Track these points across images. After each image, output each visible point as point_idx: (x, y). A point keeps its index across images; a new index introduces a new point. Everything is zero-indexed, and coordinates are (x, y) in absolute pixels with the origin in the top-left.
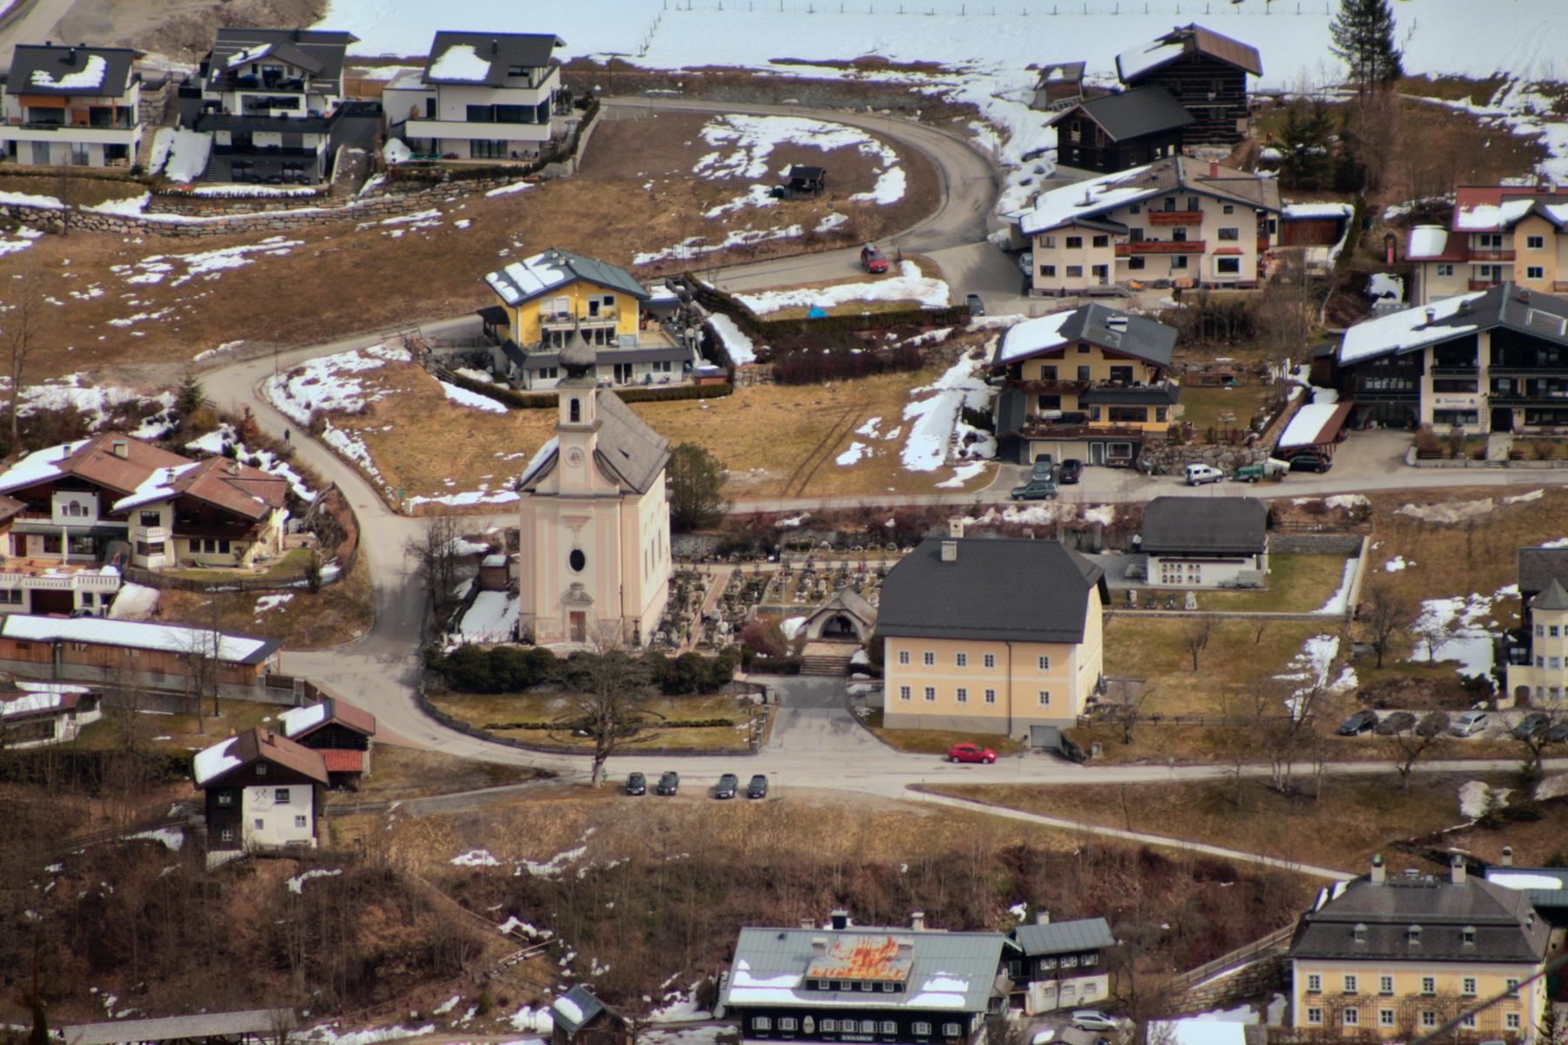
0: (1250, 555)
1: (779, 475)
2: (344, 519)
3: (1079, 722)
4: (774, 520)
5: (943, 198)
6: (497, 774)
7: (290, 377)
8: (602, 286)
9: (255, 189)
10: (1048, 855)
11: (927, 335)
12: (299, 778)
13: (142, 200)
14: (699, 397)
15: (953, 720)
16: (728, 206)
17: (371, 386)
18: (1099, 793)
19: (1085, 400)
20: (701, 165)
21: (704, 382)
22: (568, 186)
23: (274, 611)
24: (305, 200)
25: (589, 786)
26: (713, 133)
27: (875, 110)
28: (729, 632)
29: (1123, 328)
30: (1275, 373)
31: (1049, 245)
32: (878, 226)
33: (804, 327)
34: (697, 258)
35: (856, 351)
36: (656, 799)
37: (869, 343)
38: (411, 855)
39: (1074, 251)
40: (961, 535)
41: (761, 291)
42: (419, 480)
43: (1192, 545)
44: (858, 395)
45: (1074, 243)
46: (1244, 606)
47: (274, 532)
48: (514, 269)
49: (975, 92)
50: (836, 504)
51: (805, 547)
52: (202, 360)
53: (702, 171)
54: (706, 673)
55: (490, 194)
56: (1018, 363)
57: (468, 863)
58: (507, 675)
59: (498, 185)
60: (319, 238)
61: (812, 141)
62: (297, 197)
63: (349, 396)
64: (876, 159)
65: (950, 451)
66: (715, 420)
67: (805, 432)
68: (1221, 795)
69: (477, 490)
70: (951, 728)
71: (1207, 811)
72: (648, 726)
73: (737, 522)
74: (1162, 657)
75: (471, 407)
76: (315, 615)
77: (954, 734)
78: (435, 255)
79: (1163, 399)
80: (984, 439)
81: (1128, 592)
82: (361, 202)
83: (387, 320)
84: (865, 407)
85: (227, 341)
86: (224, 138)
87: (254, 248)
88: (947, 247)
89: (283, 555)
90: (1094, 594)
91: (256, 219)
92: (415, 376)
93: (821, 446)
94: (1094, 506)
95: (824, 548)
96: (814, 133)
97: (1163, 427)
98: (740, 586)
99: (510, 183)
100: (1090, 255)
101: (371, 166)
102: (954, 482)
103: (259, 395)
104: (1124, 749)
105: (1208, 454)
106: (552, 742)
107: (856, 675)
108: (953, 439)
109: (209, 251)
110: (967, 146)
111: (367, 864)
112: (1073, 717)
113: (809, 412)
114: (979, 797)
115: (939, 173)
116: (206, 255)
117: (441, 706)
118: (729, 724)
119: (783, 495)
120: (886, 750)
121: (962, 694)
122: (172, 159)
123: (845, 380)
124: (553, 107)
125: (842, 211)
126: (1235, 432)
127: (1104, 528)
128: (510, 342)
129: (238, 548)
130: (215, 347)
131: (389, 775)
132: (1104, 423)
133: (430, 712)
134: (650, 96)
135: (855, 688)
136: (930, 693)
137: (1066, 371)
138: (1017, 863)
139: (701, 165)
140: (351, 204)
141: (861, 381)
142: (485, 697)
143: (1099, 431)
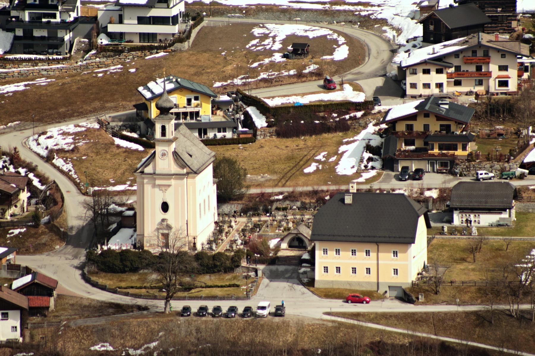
0: (505, 210)
1: (275, 177)
2: (57, 196)
3: (413, 284)
4: (270, 196)
5: (367, 58)
6: (119, 308)
7: (39, 136)
8: (192, 91)
9: (33, 57)
10: (393, 345)
12: (14, 307)
14: (239, 143)
15: (349, 283)
16: (262, 62)
17: (79, 139)
18: (421, 317)
19: (426, 140)
20: (250, 45)
21: (241, 136)
22: (185, 54)
23: (17, 236)
24: (58, 61)
25: (162, 313)
26: (257, 31)
27: (337, 22)
28: (242, 244)
29: (447, 107)
30: (525, 132)
31: (414, 73)
32: (334, 70)
33: (291, 110)
34: (245, 84)
35: (317, 122)
36: (195, 318)
37: (323, 118)
38: (69, 345)
39: (426, 76)
40: (355, 191)
41: (273, 97)
42: (97, 180)
43: (475, 205)
45: (427, 72)
46: (502, 234)
47: (21, 202)
48: (151, 85)
49: (386, 14)
50: (300, 189)
51: (285, 209)
53: (250, 47)
54: (228, 262)
55: (147, 58)
56: (394, 122)
57: (98, 349)
58: (128, 264)
59: (151, 54)
60: (63, 78)
61: (305, 34)
62: (53, 60)
63: (66, 144)
64: (336, 42)
65: (360, 165)
66: (246, 153)
67: (290, 158)
68: (484, 318)
69: (125, 184)
70: (348, 287)
71: (477, 326)
72: (196, 287)
73: (251, 197)
74: (458, 256)
75: (127, 148)
76: (37, 238)
77: (350, 290)
78: (117, 84)
79: (465, 140)
80: (376, 160)
81: (443, 227)
82: (85, 62)
83: (91, 112)
84: (321, 147)
85: (12, 122)
86: (19, 32)
87: (31, 83)
88: (366, 79)
89: (26, 214)
90: (422, 220)
91: (33, 70)
92: (100, 135)
94: (429, 189)
95: (294, 209)
96: (306, 31)
97: (466, 153)
98: (250, 225)
99: (157, 53)
100: (434, 78)
101: (91, 46)
102: (361, 180)
103: (25, 144)
104: (434, 297)
105: (488, 166)
106: (147, 294)
107: (304, 265)
108: (362, 161)
109: (9, 84)
110: (380, 37)
111: (46, 350)
112: (410, 281)
113: (292, 150)
115: (366, 48)
116: (7, 86)
117: (94, 278)
118: (238, 286)
119: (276, 186)
120: (315, 298)
121: (354, 270)
123: (311, 135)
124: (180, 19)
125: (315, 63)
126: (501, 155)
127: (433, 199)
128: (148, 119)
130: (6, 125)
131: (64, 310)
132: (436, 151)
133: (87, 280)
134: (229, 17)
135: (303, 270)
136: (338, 269)
137: (418, 126)
138: (377, 349)
139: (250, 45)
140: (80, 63)
141: (319, 136)
142: (117, 275)
143: (433, 155)
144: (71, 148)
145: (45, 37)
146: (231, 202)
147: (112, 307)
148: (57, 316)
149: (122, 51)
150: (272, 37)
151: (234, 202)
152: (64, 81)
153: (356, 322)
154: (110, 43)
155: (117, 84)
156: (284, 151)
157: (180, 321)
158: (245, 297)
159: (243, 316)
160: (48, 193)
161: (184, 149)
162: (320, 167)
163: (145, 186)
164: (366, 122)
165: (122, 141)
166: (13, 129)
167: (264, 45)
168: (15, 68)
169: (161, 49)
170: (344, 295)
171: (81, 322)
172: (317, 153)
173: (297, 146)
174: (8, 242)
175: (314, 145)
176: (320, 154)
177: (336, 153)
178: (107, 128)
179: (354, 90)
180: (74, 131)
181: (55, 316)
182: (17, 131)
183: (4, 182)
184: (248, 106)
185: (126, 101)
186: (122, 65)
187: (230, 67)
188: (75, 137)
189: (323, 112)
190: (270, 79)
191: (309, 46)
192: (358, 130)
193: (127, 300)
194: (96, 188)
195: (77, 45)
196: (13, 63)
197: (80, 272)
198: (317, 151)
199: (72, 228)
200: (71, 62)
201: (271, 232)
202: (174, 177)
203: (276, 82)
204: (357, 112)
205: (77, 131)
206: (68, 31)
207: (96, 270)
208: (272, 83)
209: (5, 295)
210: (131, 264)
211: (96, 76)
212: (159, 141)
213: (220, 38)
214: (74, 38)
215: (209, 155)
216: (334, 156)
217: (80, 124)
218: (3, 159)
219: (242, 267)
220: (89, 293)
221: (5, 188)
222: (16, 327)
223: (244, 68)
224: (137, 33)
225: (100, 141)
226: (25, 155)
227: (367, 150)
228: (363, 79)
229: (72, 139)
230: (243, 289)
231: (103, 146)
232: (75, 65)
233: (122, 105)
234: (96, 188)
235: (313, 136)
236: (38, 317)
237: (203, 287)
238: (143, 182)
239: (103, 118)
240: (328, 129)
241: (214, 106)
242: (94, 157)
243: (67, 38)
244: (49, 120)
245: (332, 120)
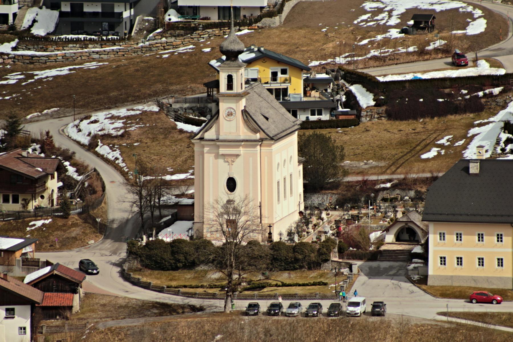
1: (382, 164)
2: (97, 185)
7: (81, 121)
9: (82, 37)
11: (487, 91)
12: (23, 301)
13: (13, 44)
15: (475, 279)
16: (373, 39)
20: (359, 20)
21: (341, 118)
22: (275, 31)
23: (40, 229)
24: (114, 42)
32: (466, 46)
35: (441, 100)
36: (264, 317)
37: (449, 95)
44: (440, 125)
52: (31, 118)
53: (359, 23)
54: (312, 255)
58: (181, 257)
65: (495, 148)
66: (346, 138)
67: (402, 143)
69: (187, 172)
70: (473, 285)
73: (350, 185)
77: (475, 288)
78: (186, 65)
82: (147, 43)
84: (445, 131)
85: (49, 109)
88: (508, 54)
92: (159, 118)
93: (411, 150)
96: (432, 4)
107: (414, 260)
108: (498, 143)
113: (407, 134)
114: (487, 320)
118: (325, 284)
119: (383, 173)
120: (428, 297)
121: (481, 262)
122: (36, 24)
125: (441, 38)
129: (24, 200)
130: (41, 112)
136: (460, 261)
139: (359, 20)
140: (141, 44)
141: (442, 119)
144: (120, 133)
145: (98, 13)
146: (324, 192)
147: (156, 307)
148: (82, 319)
149: (195, 29)
150: (388, 11)
151: (327, 192)
152: (119, 63)
153: (480, 324)
154: (180, 20)
155: (186, 65)
156: (396, 136)
157: (244, 320)
158: (333, 296)
159: (328, 315)
160: (86, 184)
161: (258, 110)
162: (443, 152)
163: (206, 155)
164: (505, 100)
165: (187, 125)
166: (49, 117)
167: (377, 20)
168: (58, 50)
169: (244, 26)
170: (467, 294)
171: (111, 323)
172: (440, 137)
173: (414, 130)
174: (28, 236)
175: (436, 128)
176: (443, 138)
177: (465, 136)
178: (168, 111)
179: (491, 67)
180: (126, 115)
181: (79, 319)
182: (55, 118)
183: (27, 165)
184: (352, 85)
185: (196, 83)
186: (194, 45)
187: (331, 45)
188: (126, 121)
189: (449, 88)
190: (382, 57)
191: (434, 18)
192: (494, 110)
193: (177, 300)
194: (148, 178)
195: (138, 24)
196: (56, 45)
197: (119, 269)
198: (439, 135)
199: (113, 221)
200: (130, 43)
201: (374, 224)
202: (243, 143)
203: (390, 60)
204: (494, 88)
205: (130, 114)
206: (128, 6)
207: (139, 266)
208: (385, 61)
209: (11, 285)
210: (186, 259)
211: (161, 57)
212: (224, 95)
213: (321, 14)
214: (135, 16)
215: (294, 122)
216: (461, 140)
217: (135, 108)
218: (32, 147)
219: (332, 261)
220: (127, 292)
221: (28, 171)
222: (25, 328)
223: (350, 45)
224: (214, 8)
225: (159, 125)
226: (59, 142)
227: (505, 130)
228: (504, 55)
229: (123, 123)
230: (332, 287)
231: (161, 130)
232: (135, 46)
233: (190, 88)
234: (148, 178)
235: (436, 118)
236: (58, 319)
237: (279, 286)
238: (203, 152)
239: (165, 101)
240: (456, 110)
241: (308, 86)
242: (148, 144)
243: (126, 14)
244: (96, 106)
245: (460, 98)
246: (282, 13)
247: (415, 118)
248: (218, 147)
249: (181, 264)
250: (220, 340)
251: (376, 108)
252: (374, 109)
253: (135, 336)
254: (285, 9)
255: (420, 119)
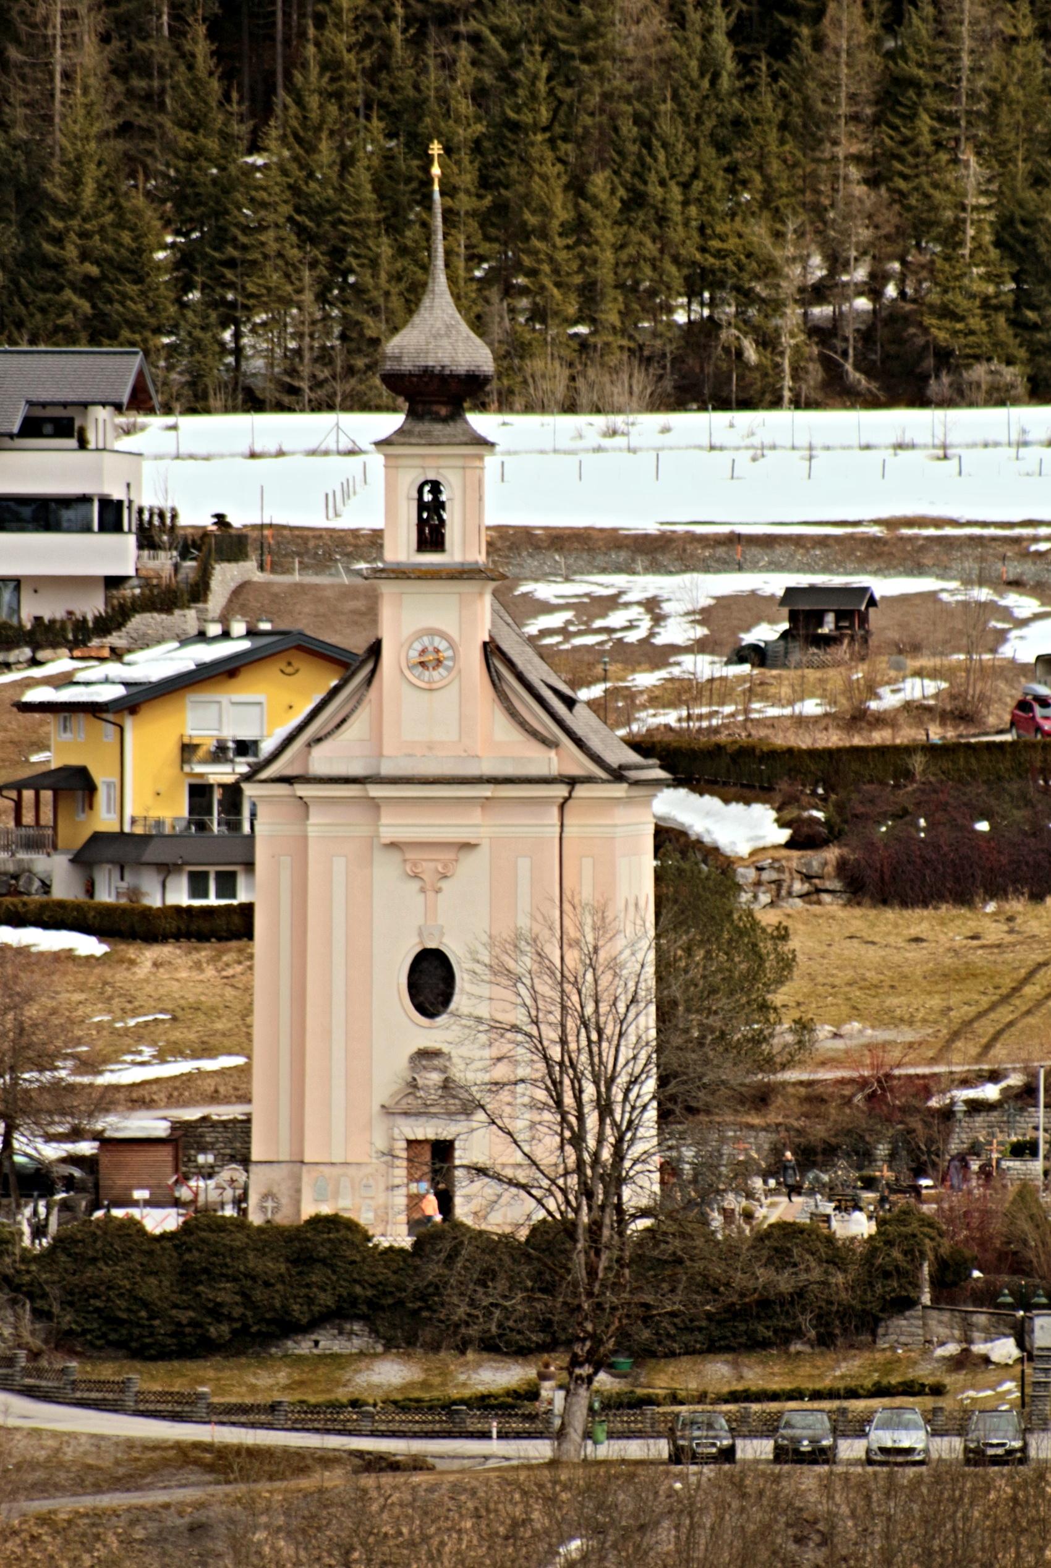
4: (928, 1094)
58: (225, 1294)
125: (919, 673)
167: (609, 630)
169: (54, 646)
173: (973, 938)
212: (401, 573)
246: (205, 601)
247: (963, 898)
248: (375, 805)
249: (225, 1328)
250: (585, 1558)
251: (795, 854)
252: (788, 859)
253: (169, 1548)
254: (214, 584)
255: (985, 902)
